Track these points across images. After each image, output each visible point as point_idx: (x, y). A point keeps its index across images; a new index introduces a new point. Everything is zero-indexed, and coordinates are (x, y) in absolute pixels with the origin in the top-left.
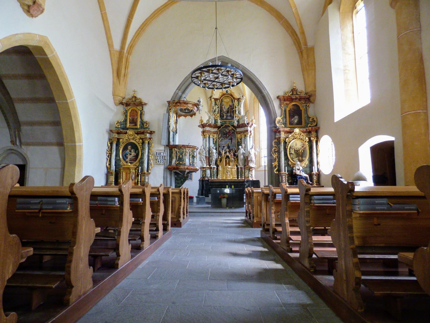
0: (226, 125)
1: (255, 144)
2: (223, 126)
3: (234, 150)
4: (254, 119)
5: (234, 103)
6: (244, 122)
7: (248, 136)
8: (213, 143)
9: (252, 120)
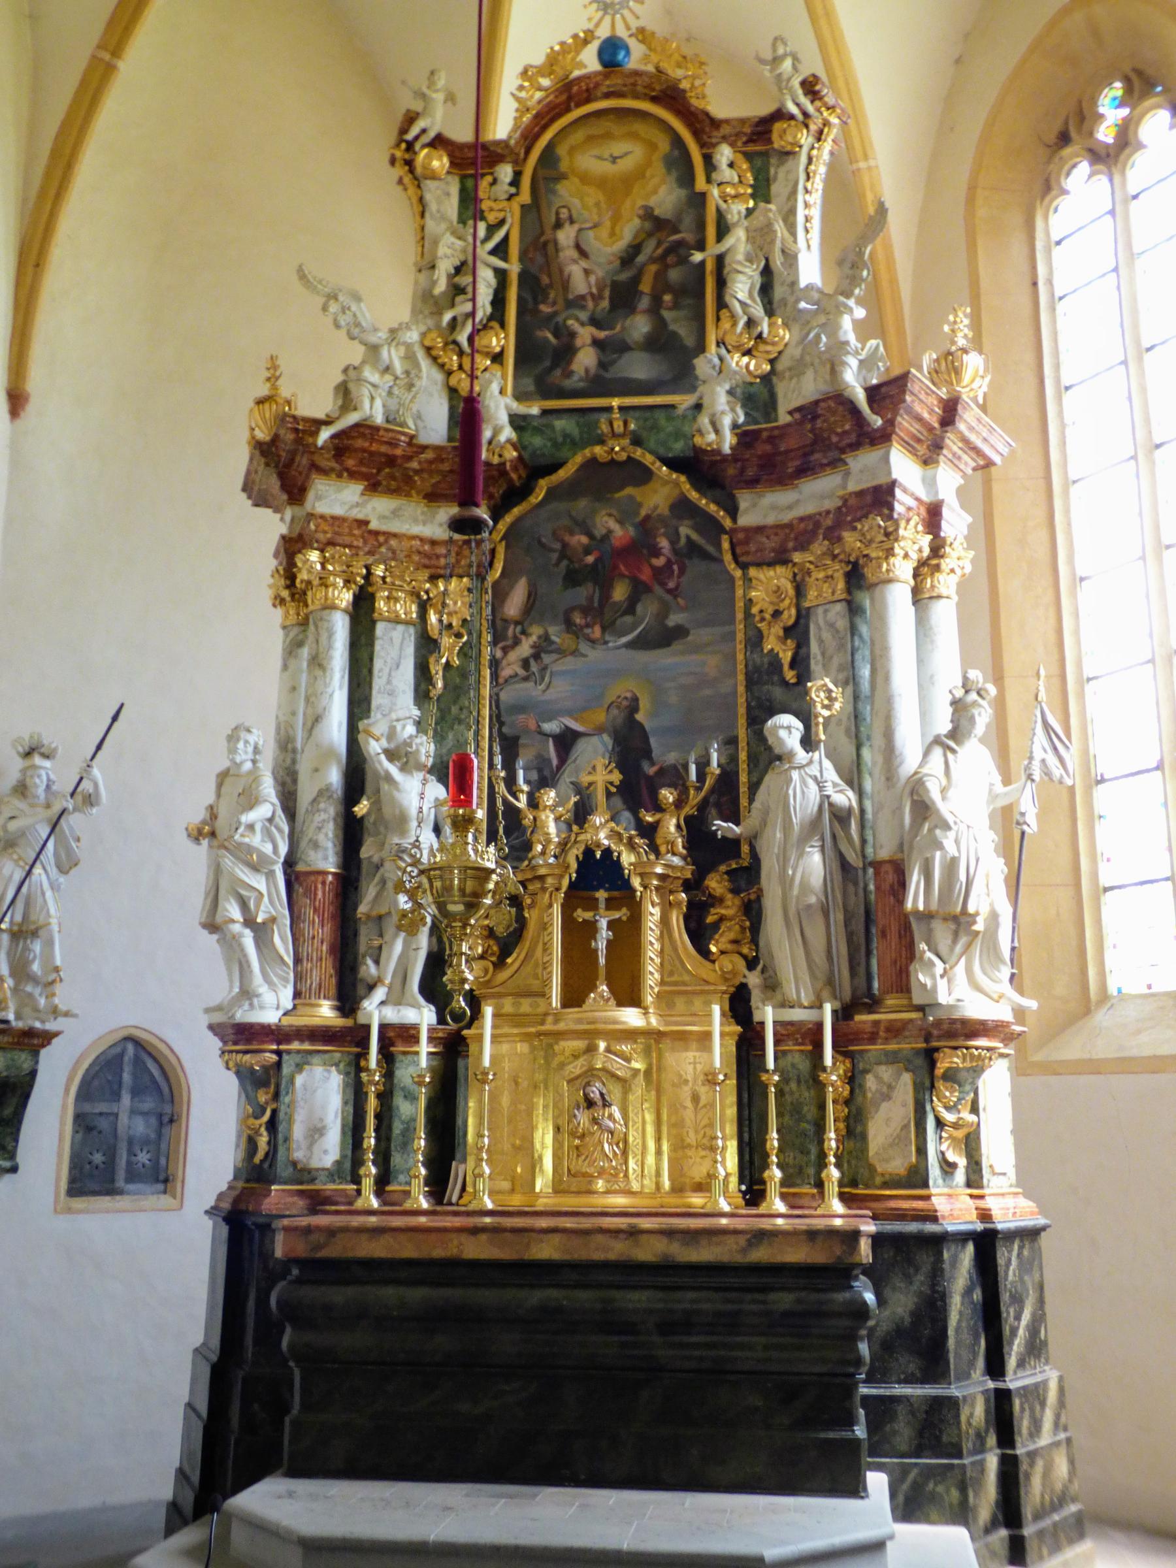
0: (593, 462)
1: (998, 678)
2: (562, 474)
3: (701, 777)
4: (977, 343)
5: (700, 184)
6: (834, 368)
7: (902, 568)
8: (422, 695)
9: (949, 365)
